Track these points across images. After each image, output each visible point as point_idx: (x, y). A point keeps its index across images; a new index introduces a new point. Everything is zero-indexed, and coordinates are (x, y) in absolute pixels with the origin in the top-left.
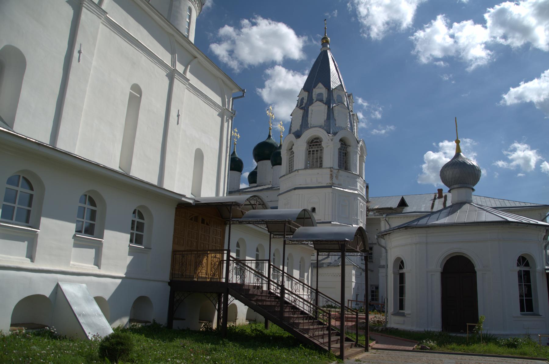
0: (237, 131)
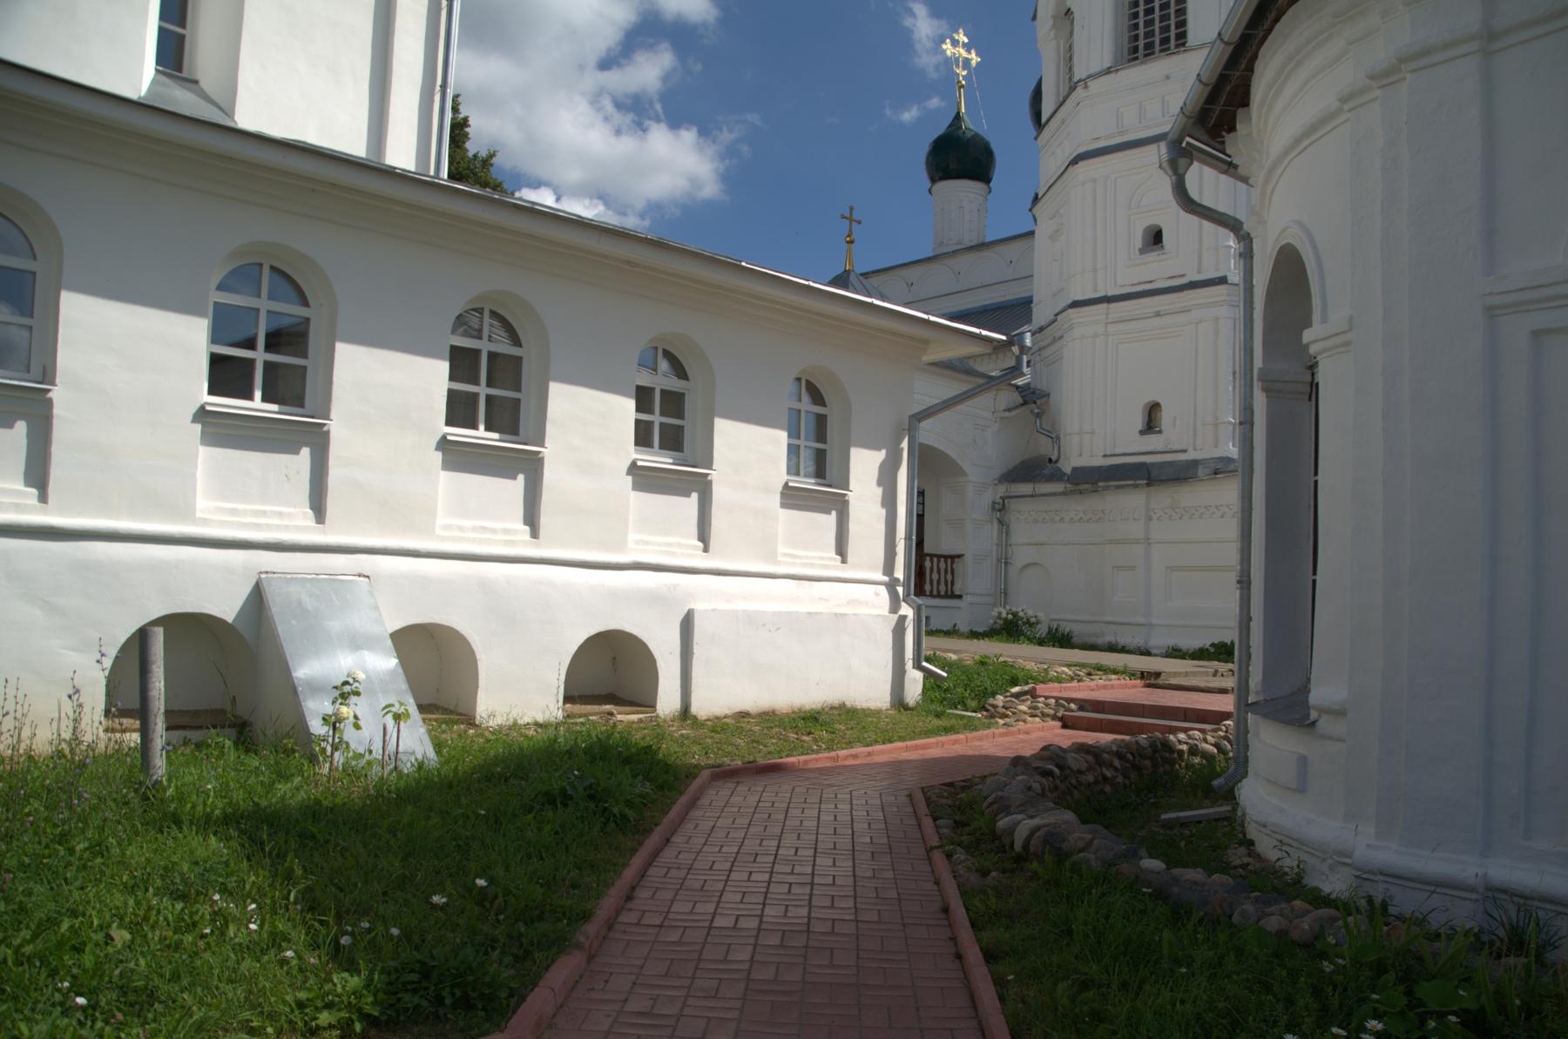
0: (966, 40)
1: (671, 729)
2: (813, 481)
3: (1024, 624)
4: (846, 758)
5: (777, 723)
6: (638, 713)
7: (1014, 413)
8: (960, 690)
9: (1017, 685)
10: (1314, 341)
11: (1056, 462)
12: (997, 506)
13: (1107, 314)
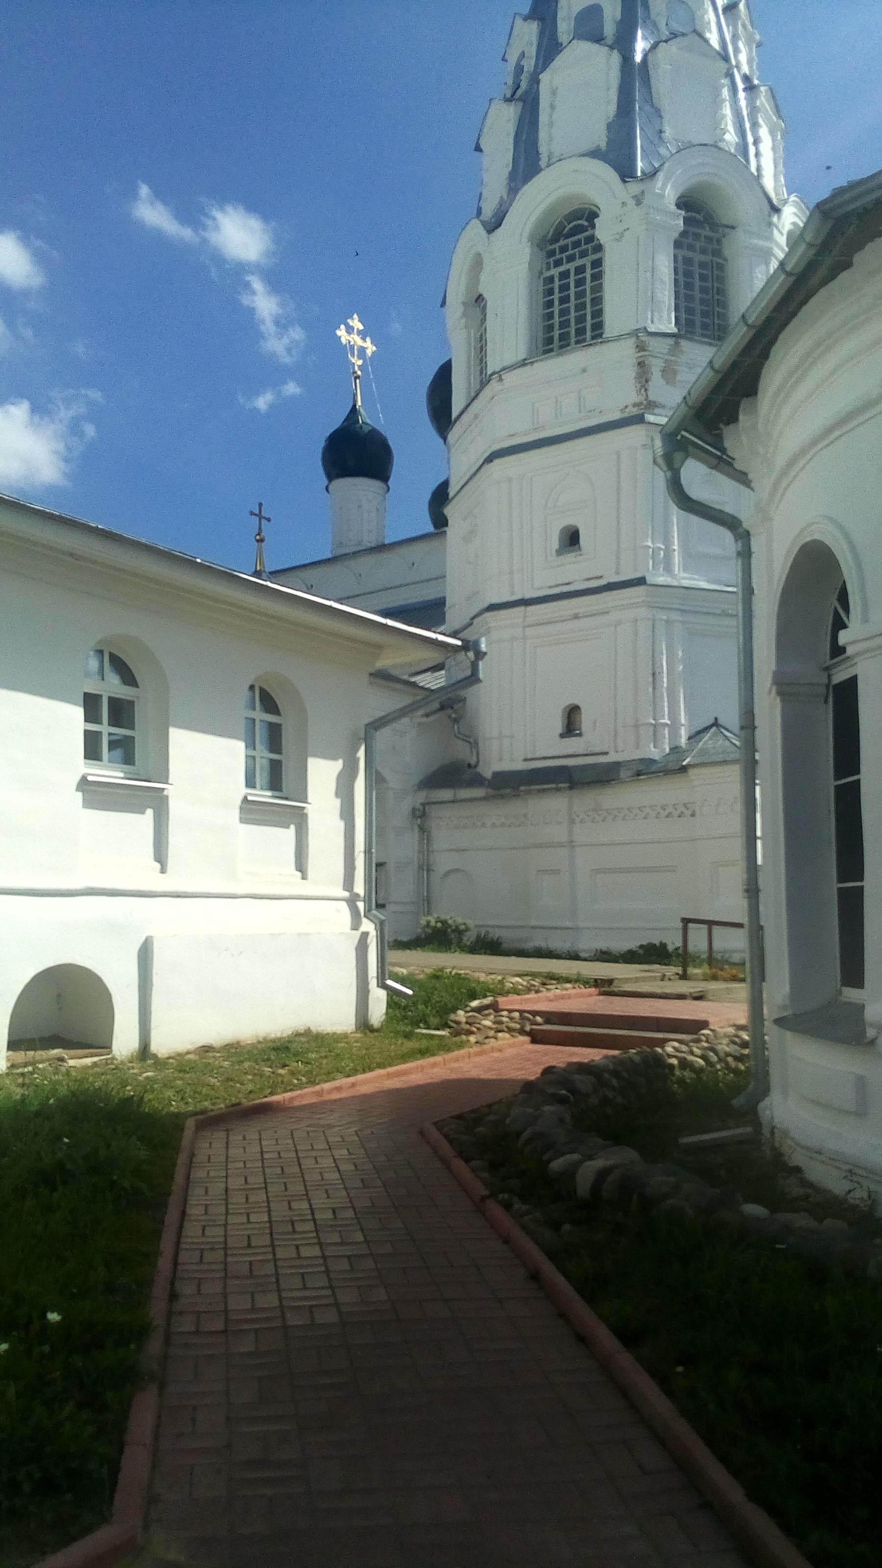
0: (361, 327)
1: (131, 1071)
2: (269, 793)
3: (453, 931)
4: (330, 1091)
5: (246, 1056)
6: (92, 1056)
7: (431, 719)
8: (421, 1007)
9: (475, 999)
10: (851, 643)
11: (476, 766)
12: (418, 813)
13: (525, 617)
